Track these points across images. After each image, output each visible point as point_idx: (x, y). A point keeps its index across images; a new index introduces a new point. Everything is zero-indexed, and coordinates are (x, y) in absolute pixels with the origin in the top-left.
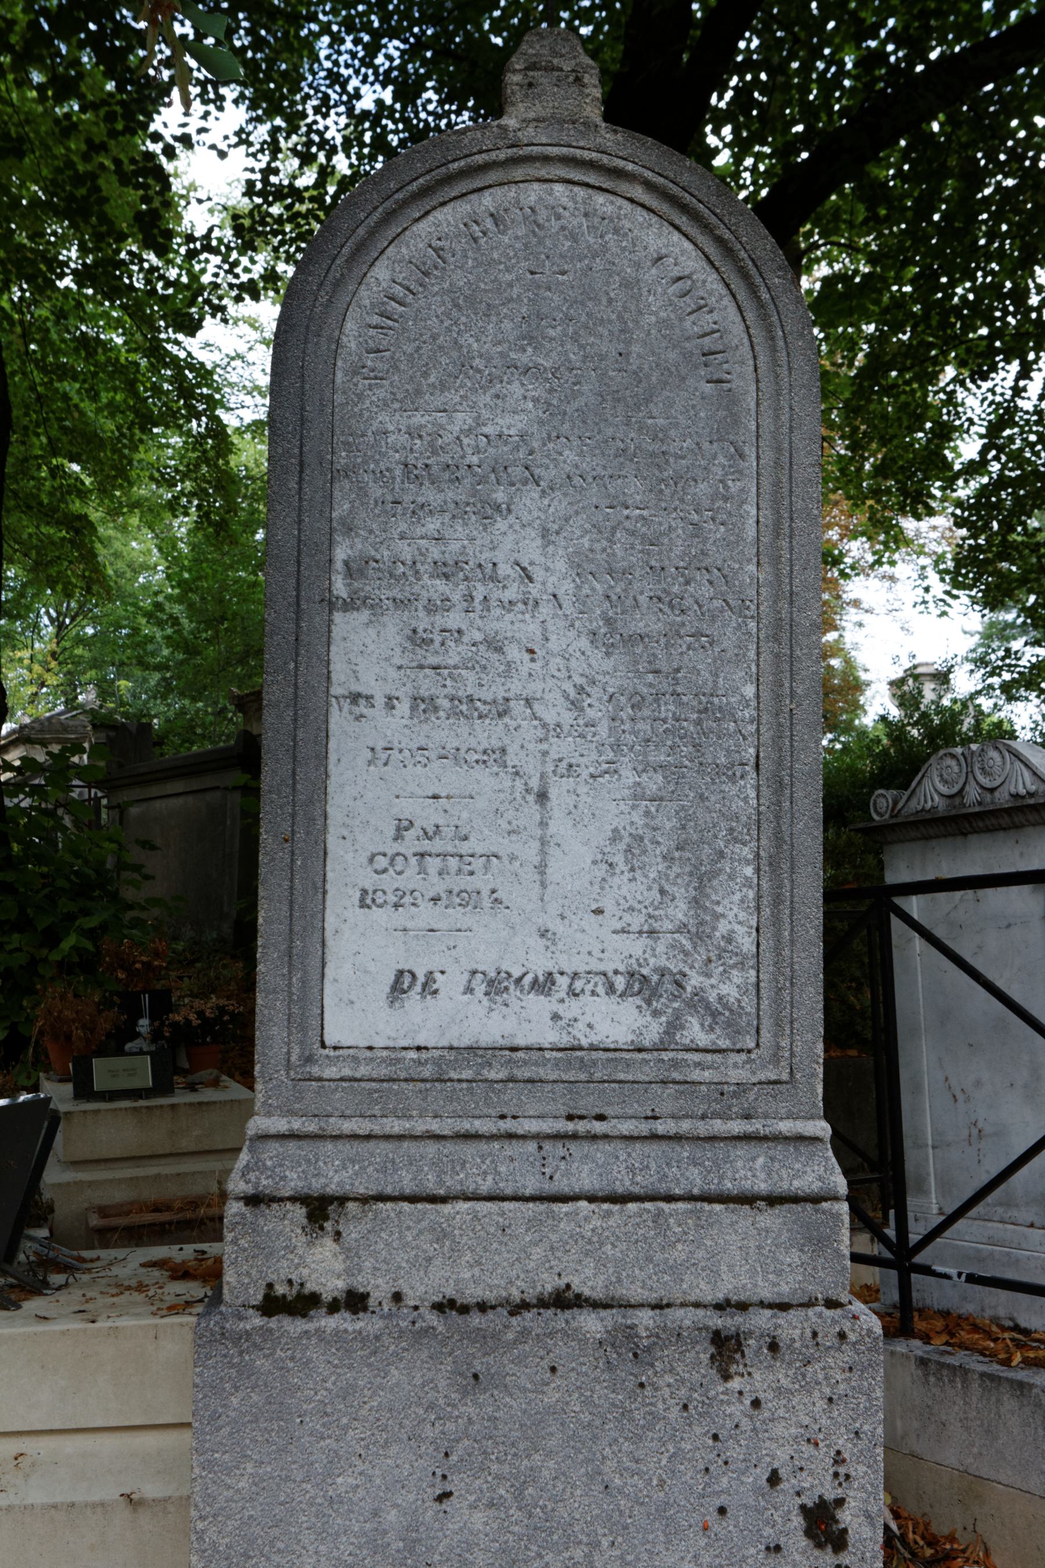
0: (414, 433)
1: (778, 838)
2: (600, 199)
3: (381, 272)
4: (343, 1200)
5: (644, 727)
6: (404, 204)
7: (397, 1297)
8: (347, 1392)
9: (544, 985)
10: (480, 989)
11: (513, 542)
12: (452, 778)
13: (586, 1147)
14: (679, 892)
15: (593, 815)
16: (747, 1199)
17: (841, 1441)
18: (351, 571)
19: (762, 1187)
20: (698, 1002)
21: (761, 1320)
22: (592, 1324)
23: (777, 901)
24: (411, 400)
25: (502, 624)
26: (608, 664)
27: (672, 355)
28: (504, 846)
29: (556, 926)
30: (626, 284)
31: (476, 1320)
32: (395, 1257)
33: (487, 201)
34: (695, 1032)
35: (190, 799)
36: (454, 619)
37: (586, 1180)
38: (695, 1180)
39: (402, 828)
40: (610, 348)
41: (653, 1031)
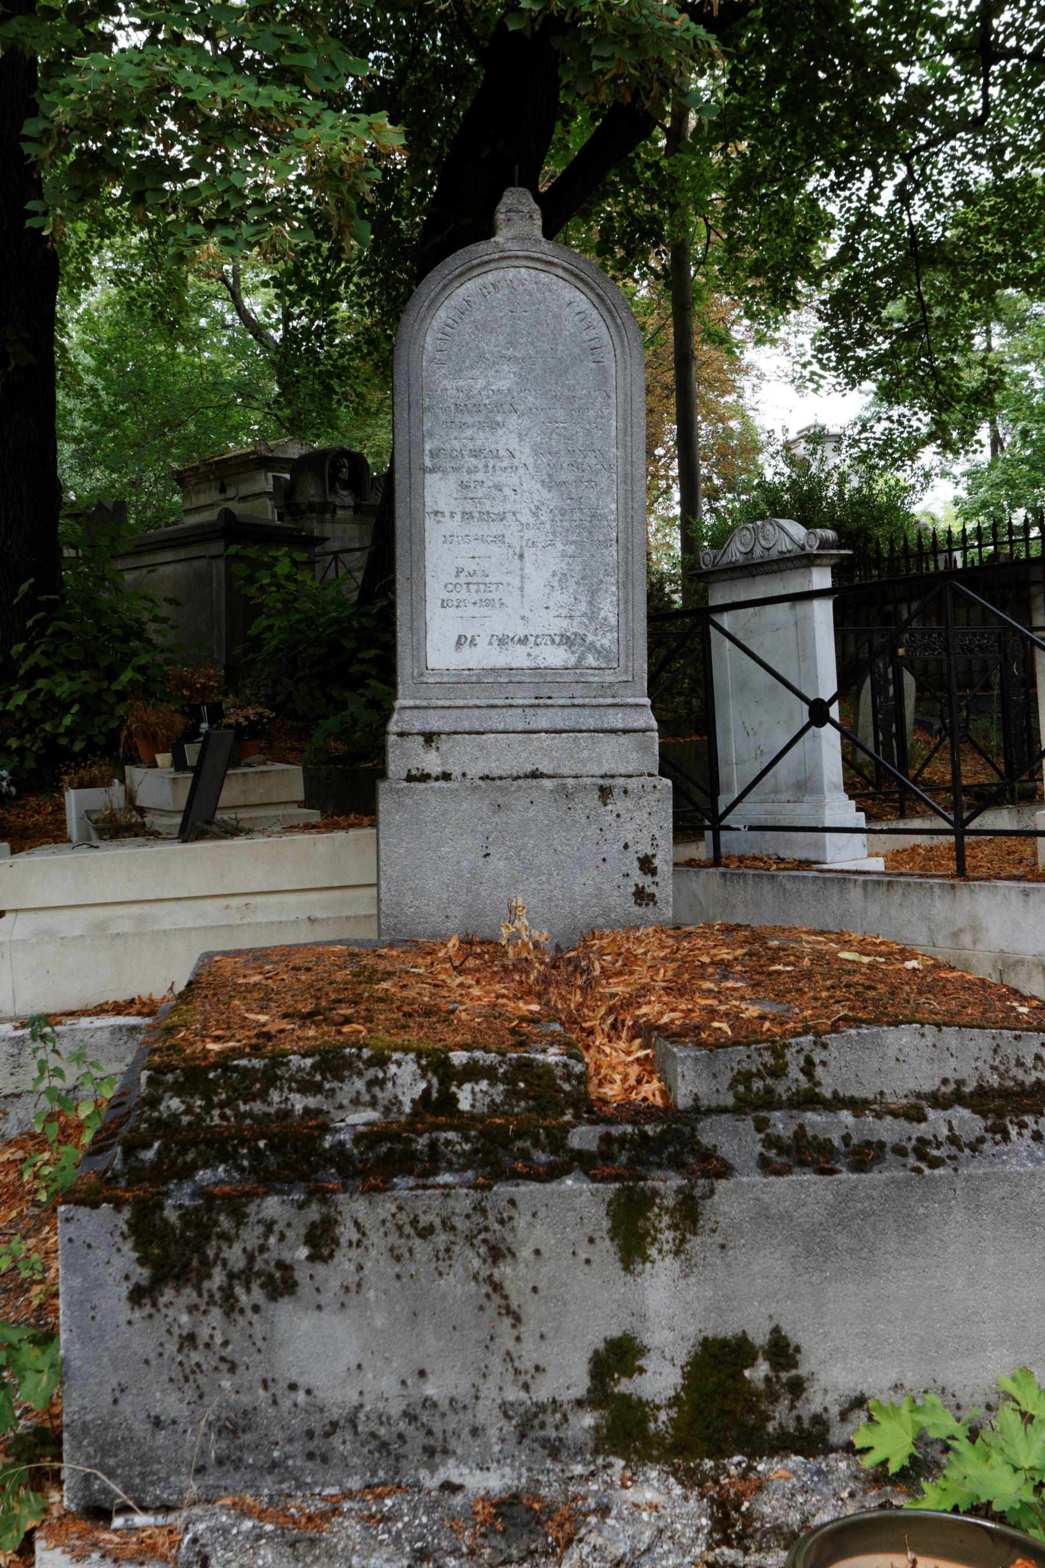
0: (459, 389)
1: (627, 573)
2: (542, 275)
3: (442, 313)
4: (439, 734)
5: (566, 524)
6: (452, 281)
7: (464, 775)
8: (445, 813)
9: (523, 641)
10: (495, 643)
11: (506, 440)
12: (480, 549)
13: (544, 710)
14: (582, 598)
15: (545, 563)
16: (614, 731)
17: (655, 831)
18: (432, 455)
19: (620, 726)
20: (592, 647)
21: (621, 781)
22: (548, 783)
23: (626, 602)
24: (458, 373)
25: (501, 478)
26: (549, 496)
27: (577, 350)
28: (505, 579)
29: (529, 615)
30: (555, 317)
31: (498, 782)
32: (462, 757)
33: (490, 277)
34: (591, 660)
35: (179, 567)
36: (480, 476)
37: (544, 724)
38: (591, 723)
39: (459, 572)
40: (547, 347)
41: (572, 661)
